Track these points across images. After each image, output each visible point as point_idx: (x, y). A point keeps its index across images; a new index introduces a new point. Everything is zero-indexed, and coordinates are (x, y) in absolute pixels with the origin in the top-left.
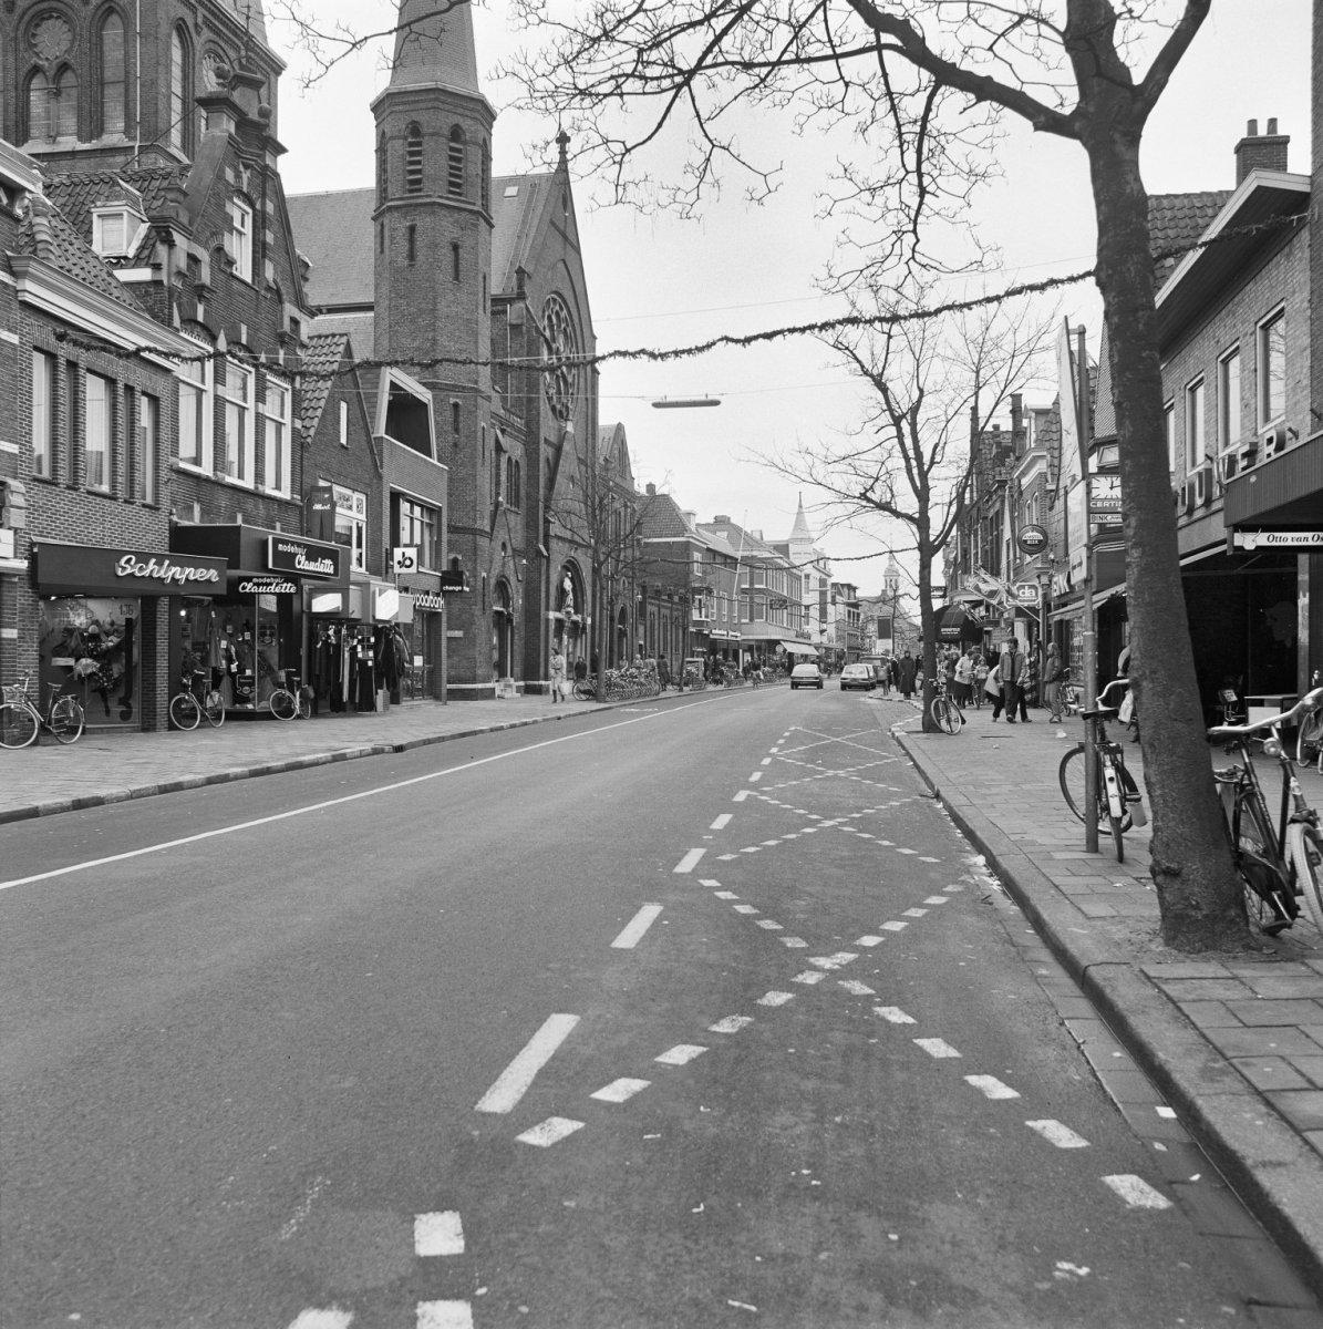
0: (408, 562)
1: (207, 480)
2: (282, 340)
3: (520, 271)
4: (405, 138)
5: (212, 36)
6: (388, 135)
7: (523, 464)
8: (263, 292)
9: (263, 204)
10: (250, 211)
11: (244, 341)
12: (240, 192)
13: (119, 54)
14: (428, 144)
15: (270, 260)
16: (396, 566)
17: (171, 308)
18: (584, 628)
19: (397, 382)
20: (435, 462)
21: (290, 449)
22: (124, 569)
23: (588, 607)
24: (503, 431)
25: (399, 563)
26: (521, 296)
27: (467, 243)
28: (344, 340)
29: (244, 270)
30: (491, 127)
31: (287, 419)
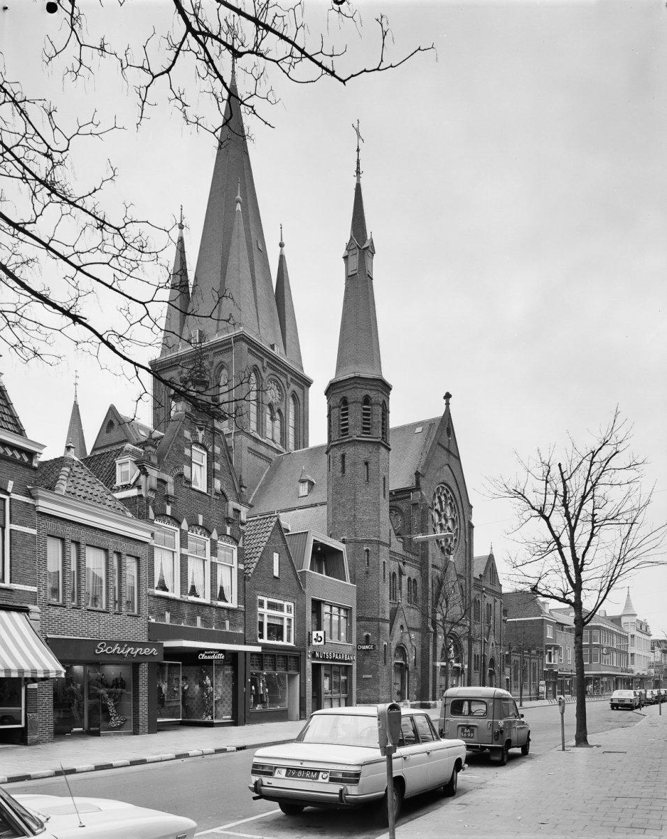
0: (319, 639)
1: (174, 600)
2: (228, 521)
3: (417, 474)
4: (339, 407)
5: (272, 371)
7: (419, 581)
8: (213, 496)
9: (213, 448)
10: (206, 453)
11: (201, 524)
12: (197, 443)
14: (352, 408)
15: (218, 478)
16: (314, 641)
17: (148, 509)
18: (463, 671)
20: (349, 583)
21: (236, 578)
23: (466, 658)
24: (404, 563)
25: (315, 639)
27: (373, 460)
28: (275, 519)
29: (200, 484)
31: (235, 564)
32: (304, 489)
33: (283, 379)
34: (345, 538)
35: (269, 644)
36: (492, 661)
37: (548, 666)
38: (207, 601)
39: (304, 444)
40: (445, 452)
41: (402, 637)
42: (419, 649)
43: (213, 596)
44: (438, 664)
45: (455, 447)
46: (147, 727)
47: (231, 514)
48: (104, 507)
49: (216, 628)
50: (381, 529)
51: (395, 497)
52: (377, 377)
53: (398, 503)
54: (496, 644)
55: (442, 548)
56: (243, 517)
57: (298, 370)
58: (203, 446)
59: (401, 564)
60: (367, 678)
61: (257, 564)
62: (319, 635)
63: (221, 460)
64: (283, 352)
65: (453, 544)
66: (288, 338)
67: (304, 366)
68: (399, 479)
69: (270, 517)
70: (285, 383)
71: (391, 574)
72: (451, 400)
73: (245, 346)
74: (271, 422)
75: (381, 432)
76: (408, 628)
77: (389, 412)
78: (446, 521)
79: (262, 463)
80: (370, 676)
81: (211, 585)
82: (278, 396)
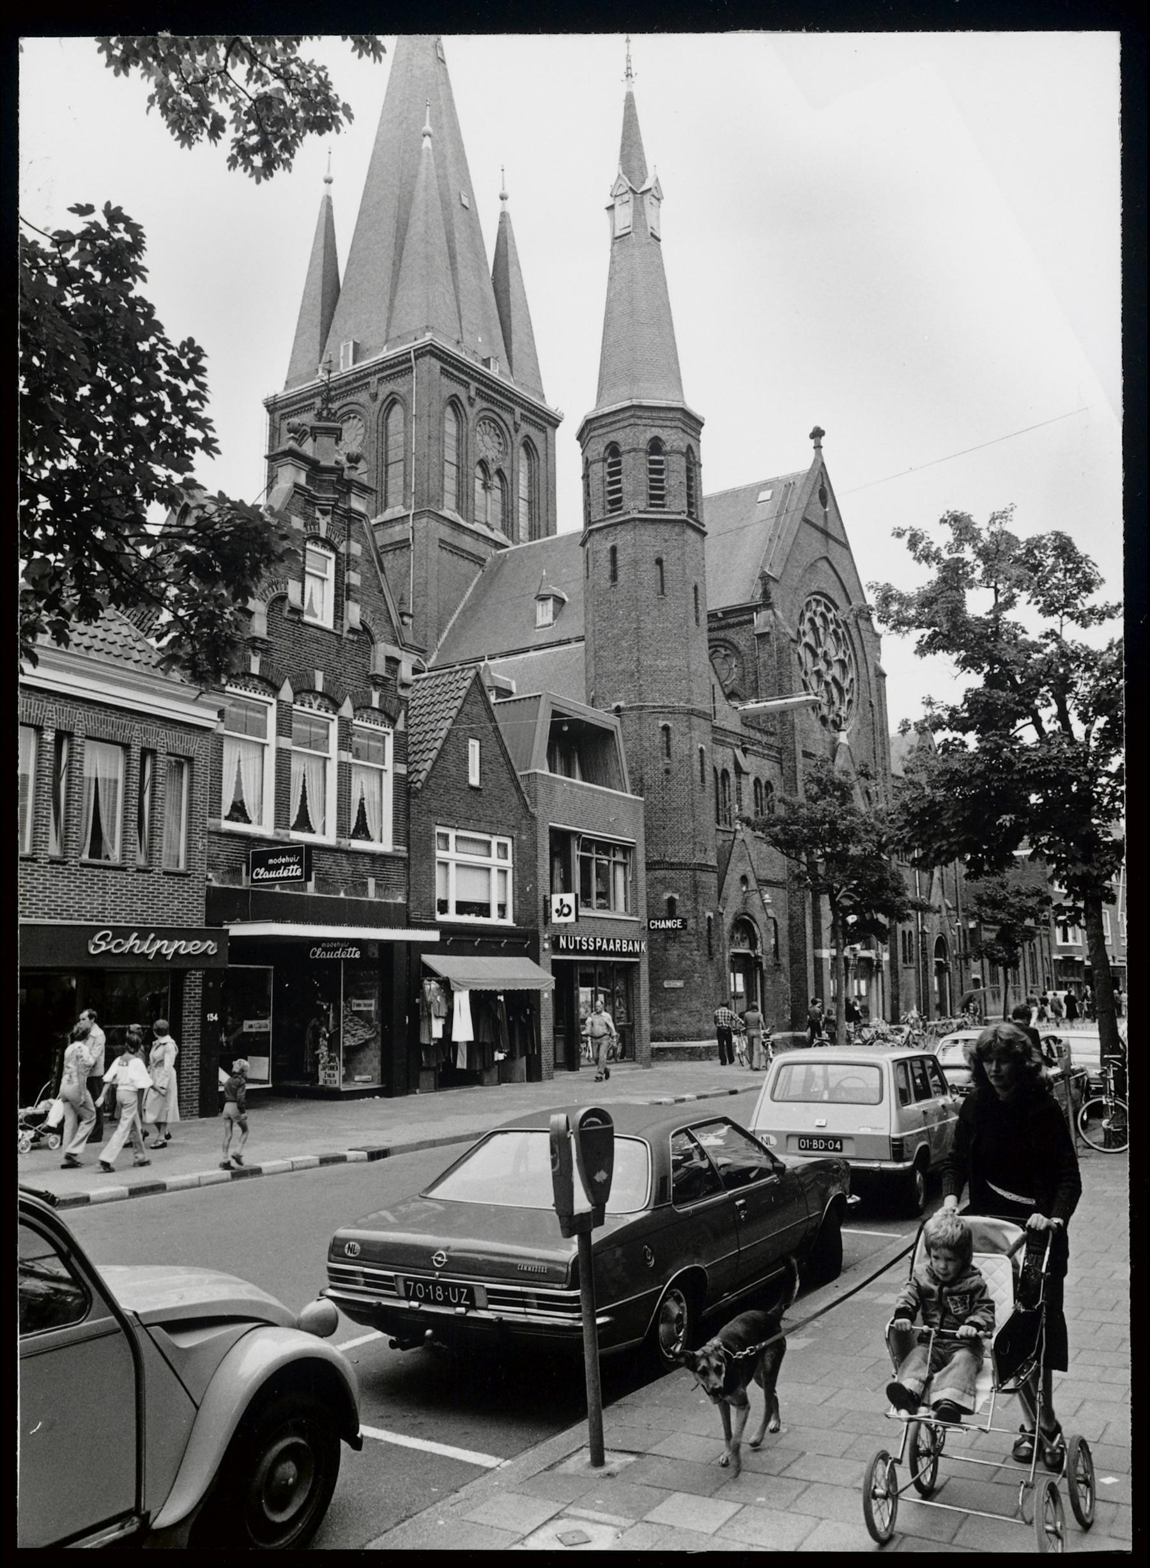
2: (375, 681)
3: (765, 578)
4: (604, 460)
5: (485, 405)
6: (590, 459)
9: (348, 547)
10: (332, 555)
11: (319, 688)
12: (316, 539)
13: (400, 438)
14: (627, 461)
15: (356, 601)
16: (554, 915)
18: (879, 966)
19: (558, 709)
22: (97, 946)
24: (745, 751)
25: (557, 911)
26: (767, 603)
28: (472, 673)
29: (322, 614)
30: (699, 433)
32: (545, 613)
33: (506, 416)
34: (622, 704)
35: (460, 924)
36: (941, 945)
37: (1062, 949)
38: (330, 838)
39: (547, 529)
40: (817, 535)
41: (745, 902)
42: (783, 923)
43: (342, 830)
44: (826, 953)
45: (838, 523)
46: (196, 1104)
47: (379, 667)
48: (130, 665)
49: (346, 894)
50: (694, 686)
51: (723, 623)
52: (674, 404)
53: (731, 634)
54: (948, 909)
55: (824, 720)
56: (405, 672)
57: (535, 400)
58: (328, 543)
59: (739, 752)
60: (674, 989)
61: (435, 763)
62: (565, 902)
63: (365, 567)
64: (507, 370)
65: (844, 708)
66: (515, 347)
67: (545, 392)
68: (728, 588)
69: (463, 670)
70: (510, 423)
71: (719, 772)
72: (824, 441)
73: (437, 365)
74: (483, 492)
75: (685, 502)
76: (758, 881)
77: (700, 466)
78: (829, 664)
79: (465, 566)
80: (679, 984)
81: (339, 807)
82: (497, 445)
